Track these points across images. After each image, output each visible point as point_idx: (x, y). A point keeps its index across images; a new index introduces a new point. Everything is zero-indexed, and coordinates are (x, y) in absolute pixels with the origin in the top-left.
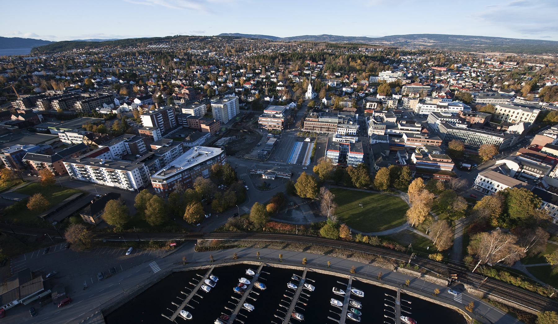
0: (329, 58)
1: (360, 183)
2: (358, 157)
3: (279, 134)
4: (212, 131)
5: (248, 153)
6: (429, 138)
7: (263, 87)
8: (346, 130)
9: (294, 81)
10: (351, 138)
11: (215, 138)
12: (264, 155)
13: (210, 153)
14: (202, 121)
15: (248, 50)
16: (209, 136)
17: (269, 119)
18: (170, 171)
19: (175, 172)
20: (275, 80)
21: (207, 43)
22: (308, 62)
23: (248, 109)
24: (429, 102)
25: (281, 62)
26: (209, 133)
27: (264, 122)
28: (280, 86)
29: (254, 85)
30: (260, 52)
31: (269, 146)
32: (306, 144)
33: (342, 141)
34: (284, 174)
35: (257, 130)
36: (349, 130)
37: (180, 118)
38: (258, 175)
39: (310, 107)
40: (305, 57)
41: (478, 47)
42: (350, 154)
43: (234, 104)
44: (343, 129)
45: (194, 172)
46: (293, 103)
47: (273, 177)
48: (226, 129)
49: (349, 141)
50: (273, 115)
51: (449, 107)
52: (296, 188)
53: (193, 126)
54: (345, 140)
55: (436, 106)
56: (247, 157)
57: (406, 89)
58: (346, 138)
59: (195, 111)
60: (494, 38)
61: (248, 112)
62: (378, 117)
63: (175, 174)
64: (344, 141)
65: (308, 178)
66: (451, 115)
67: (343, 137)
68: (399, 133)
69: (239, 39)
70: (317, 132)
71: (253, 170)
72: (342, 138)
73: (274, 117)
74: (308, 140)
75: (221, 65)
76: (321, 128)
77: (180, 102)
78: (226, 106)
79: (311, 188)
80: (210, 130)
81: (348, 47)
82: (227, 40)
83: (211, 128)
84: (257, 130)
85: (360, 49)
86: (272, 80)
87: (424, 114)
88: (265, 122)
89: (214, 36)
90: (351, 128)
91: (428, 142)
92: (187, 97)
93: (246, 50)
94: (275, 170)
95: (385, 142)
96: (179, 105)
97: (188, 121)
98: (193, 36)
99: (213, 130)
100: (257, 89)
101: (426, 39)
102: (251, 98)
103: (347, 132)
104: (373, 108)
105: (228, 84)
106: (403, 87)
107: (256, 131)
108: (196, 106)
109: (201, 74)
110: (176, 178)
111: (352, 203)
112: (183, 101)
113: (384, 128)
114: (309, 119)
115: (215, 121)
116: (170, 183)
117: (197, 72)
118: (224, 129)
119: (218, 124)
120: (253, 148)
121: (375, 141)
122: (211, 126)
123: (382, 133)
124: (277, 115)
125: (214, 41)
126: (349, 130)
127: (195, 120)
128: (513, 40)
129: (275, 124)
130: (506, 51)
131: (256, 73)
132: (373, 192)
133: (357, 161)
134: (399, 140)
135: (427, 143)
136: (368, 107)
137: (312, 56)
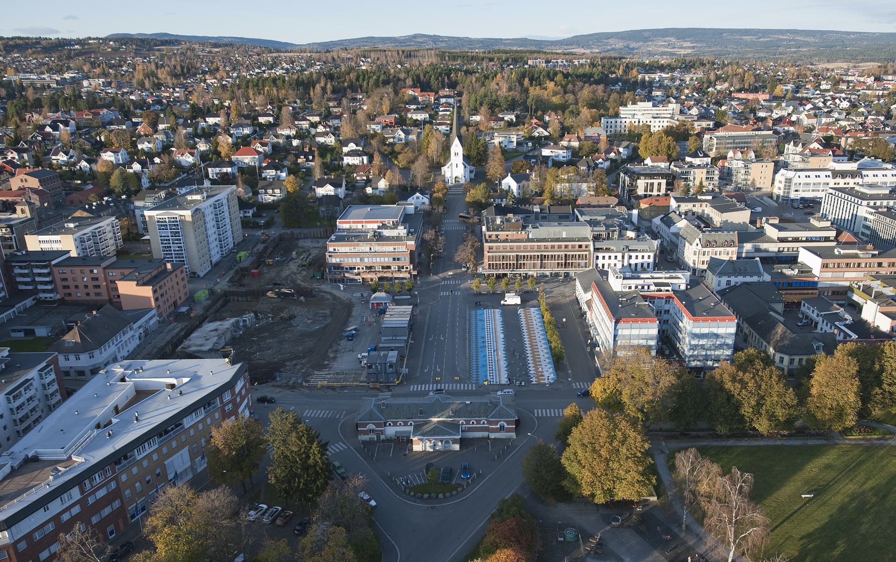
0: (468, 80)
1: (772, 417)
2: (721, 331)
3: (410, 290)
4: (160, 302)
5: (320, 367)
6: (880, 255)
7: (300, 161)
8: (623, 257)
9: (391, 140)
10: (668, 275)
11: (177, 328)
12: (391, 366)
13: (185, 380)
14: (113, 273)
15: (213, 72)
16: (152, 322)
17: (364, 247)
18: (19, 481)
19: (48, 483)
20: (330, 140)
21: (69, 58)
22: (411, 92)
23: (268, 225)
24: (801, 166)
25: (329, 94)
26: (154, 312)
27: (348, 257)
28: (352, 153)
29: (266, 156)
30: (250, 75)
31: (394, 331)
32: (510, 314)
33: (643, 287)
34: (490, 423)
35: (326, 287)
36: (630, 257)
37: (21, 267)
38: (389, 440)
39: (475, 202)
40: (399, 80)
41: (795, 52)
42: (687, 325)
43: (226, 208)
44: (613, 255)
45: (135, 470)
46: (418, 194)
47: (455, 442)
48: (212, 292)
49: (667, 285)
50: (375, 232)
51: (864, 173)
52: (572, 468)
53: (80, 295)
54: (656, 284)
55: (829, 173)
56: (320, 379)
57: (715, 141)
58: (653, 278)
59: (81, 241)
60: (823, 33)
61: (273, 232)
62: (690, 214)
63: (47, 489)
64: (653, 288)
65: (616, 426)
66: (887, 192)
67: (642, 276)
68: (776, 250)
69: (174, 45)
70: (530, 273)
71: (371, 426)
72: (639, 278)
73: (378, 237)
74: (512, 299)
75: (136, 108)
76: (543, 258)
77: (14, 216)
78: (199, 215)
79: (634, 462)
80: (156, 300)
81: (498, 59)
82: (136, 50)
83: (159, 292)
84: (326, 287)
85: (530, 62)
86: (321, 140)
87: (802, 199)
88: (352, 257)
89: (90, 38)
90: (636, 251)
91: (880, 265)
92: (35, 199)
93: (204, 73)
94: (457, 413)
95: (755, 279)
96: (10, 227)
97: (58, 277)
98: (20, 38)
99: (165, 298)
100: (284, 167)
101: (673, 40)
102: (270, 191)
103: (626, 264)
104: (655, 193)
105: (179, 157)
106: (706, 137)
107: (320, 291)
108: (82, 223)
109: (72, 134)
110: (55, 507)
111: (775, 495)
112: (23, 211)
113: (733, 241)
114: (497, 236)
115: (169, 266)
116: (28, 537)
117: (55, 127)
118: (202, 295)
119: (180, 276)
120: (331, 347)
121: (724, 279)
122: (157, 287)
123: (728, 254)
124: (386, 233)
125: (95, 52)
126: (630, 257)
127: (87, 270)
128: (862, 36)
129: (387, 260)
130: (859, 58)
131: (261, 125)
132: (811, 442)
133: (721, 347)
134: (797, 271)
135: (879, 269)
136: (640, 192)
137: (418, 76)
